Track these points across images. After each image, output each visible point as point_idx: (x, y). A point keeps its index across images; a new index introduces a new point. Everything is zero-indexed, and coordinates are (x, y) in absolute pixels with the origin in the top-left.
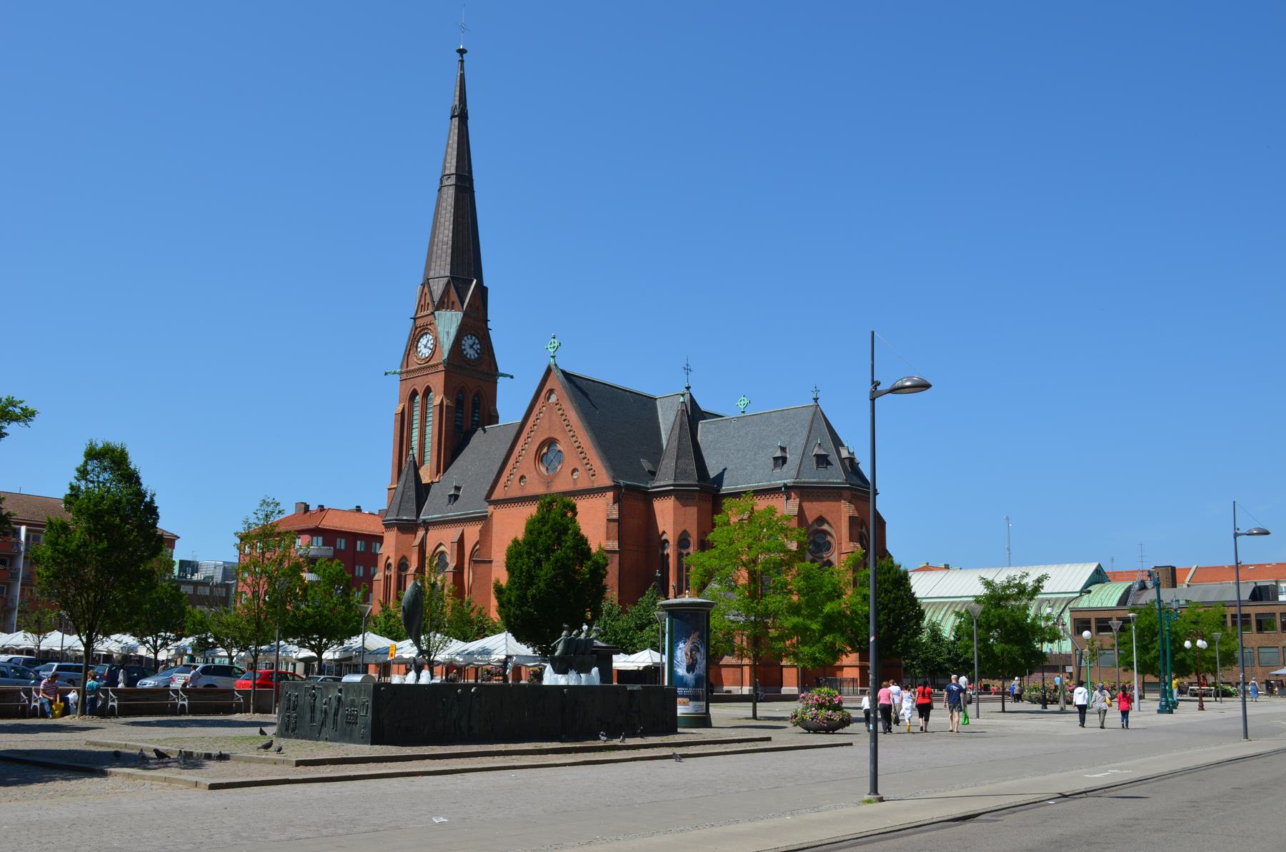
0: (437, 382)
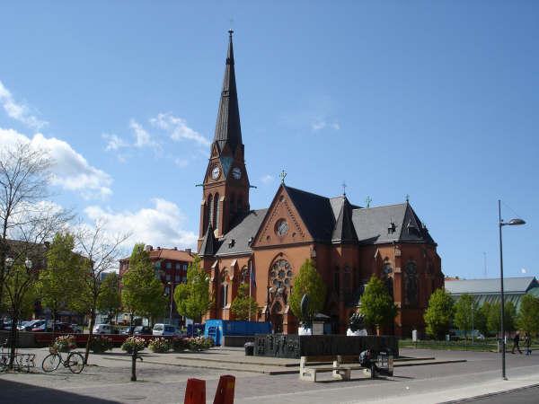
0: (222, 190)
